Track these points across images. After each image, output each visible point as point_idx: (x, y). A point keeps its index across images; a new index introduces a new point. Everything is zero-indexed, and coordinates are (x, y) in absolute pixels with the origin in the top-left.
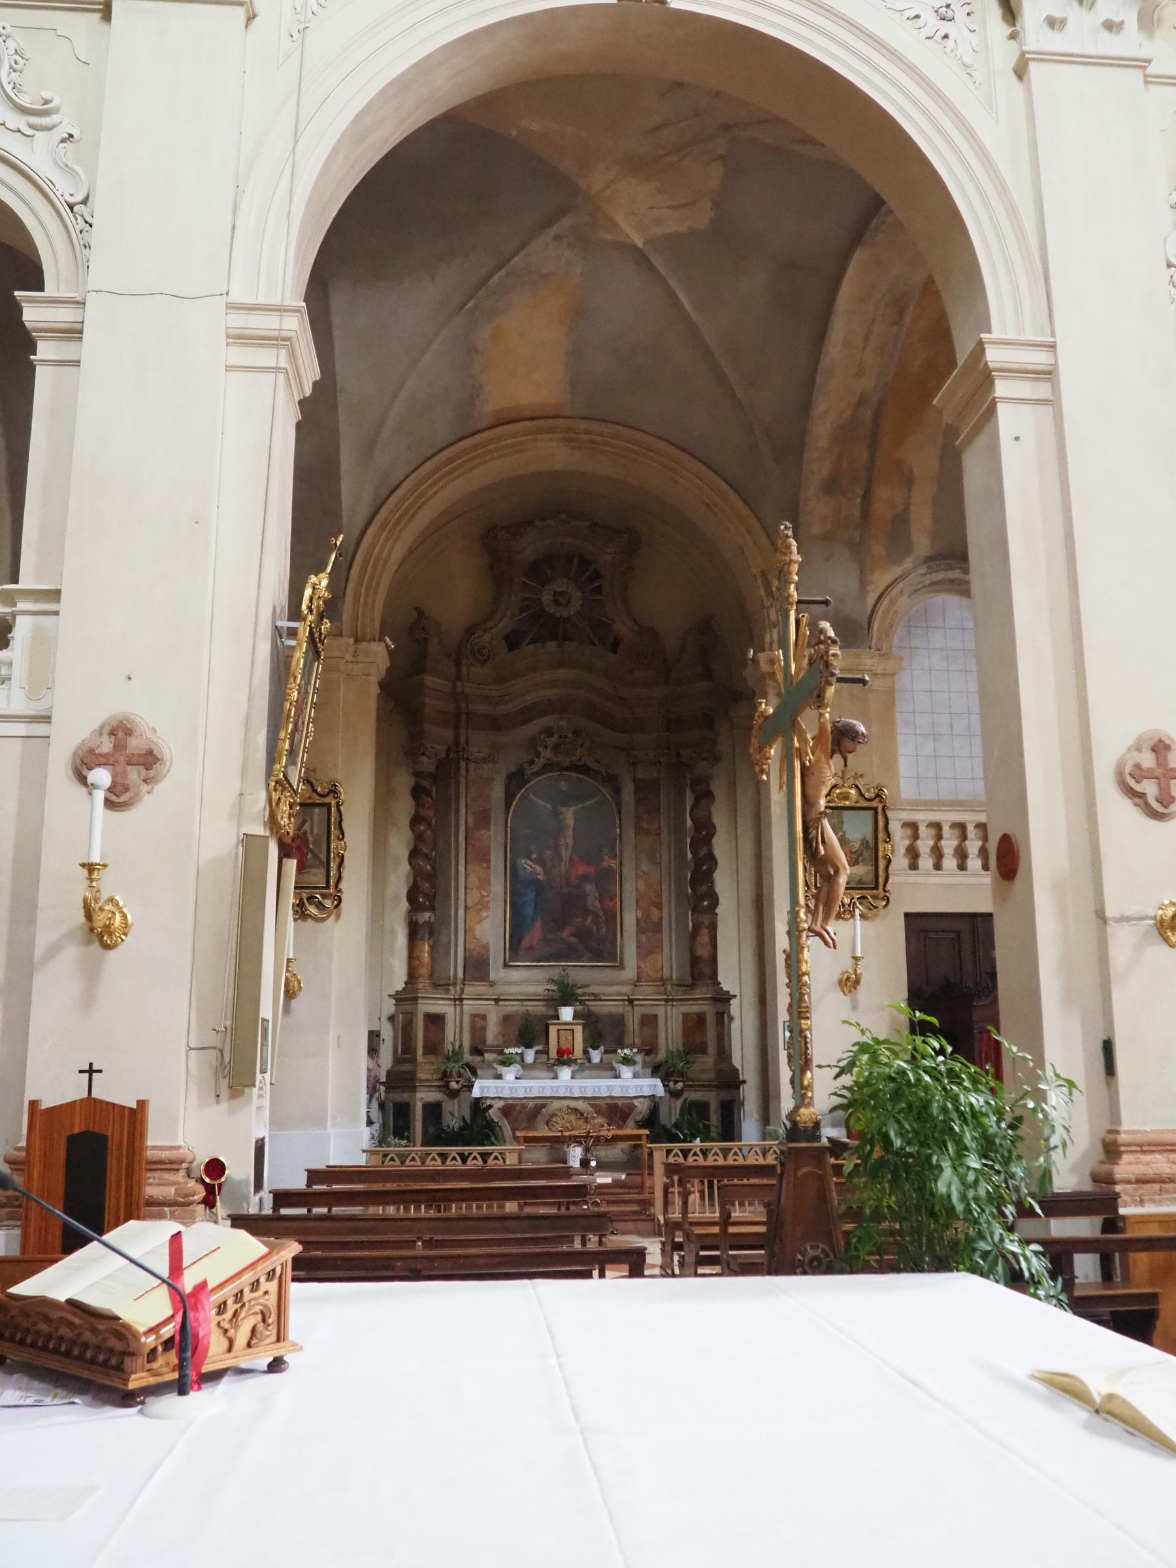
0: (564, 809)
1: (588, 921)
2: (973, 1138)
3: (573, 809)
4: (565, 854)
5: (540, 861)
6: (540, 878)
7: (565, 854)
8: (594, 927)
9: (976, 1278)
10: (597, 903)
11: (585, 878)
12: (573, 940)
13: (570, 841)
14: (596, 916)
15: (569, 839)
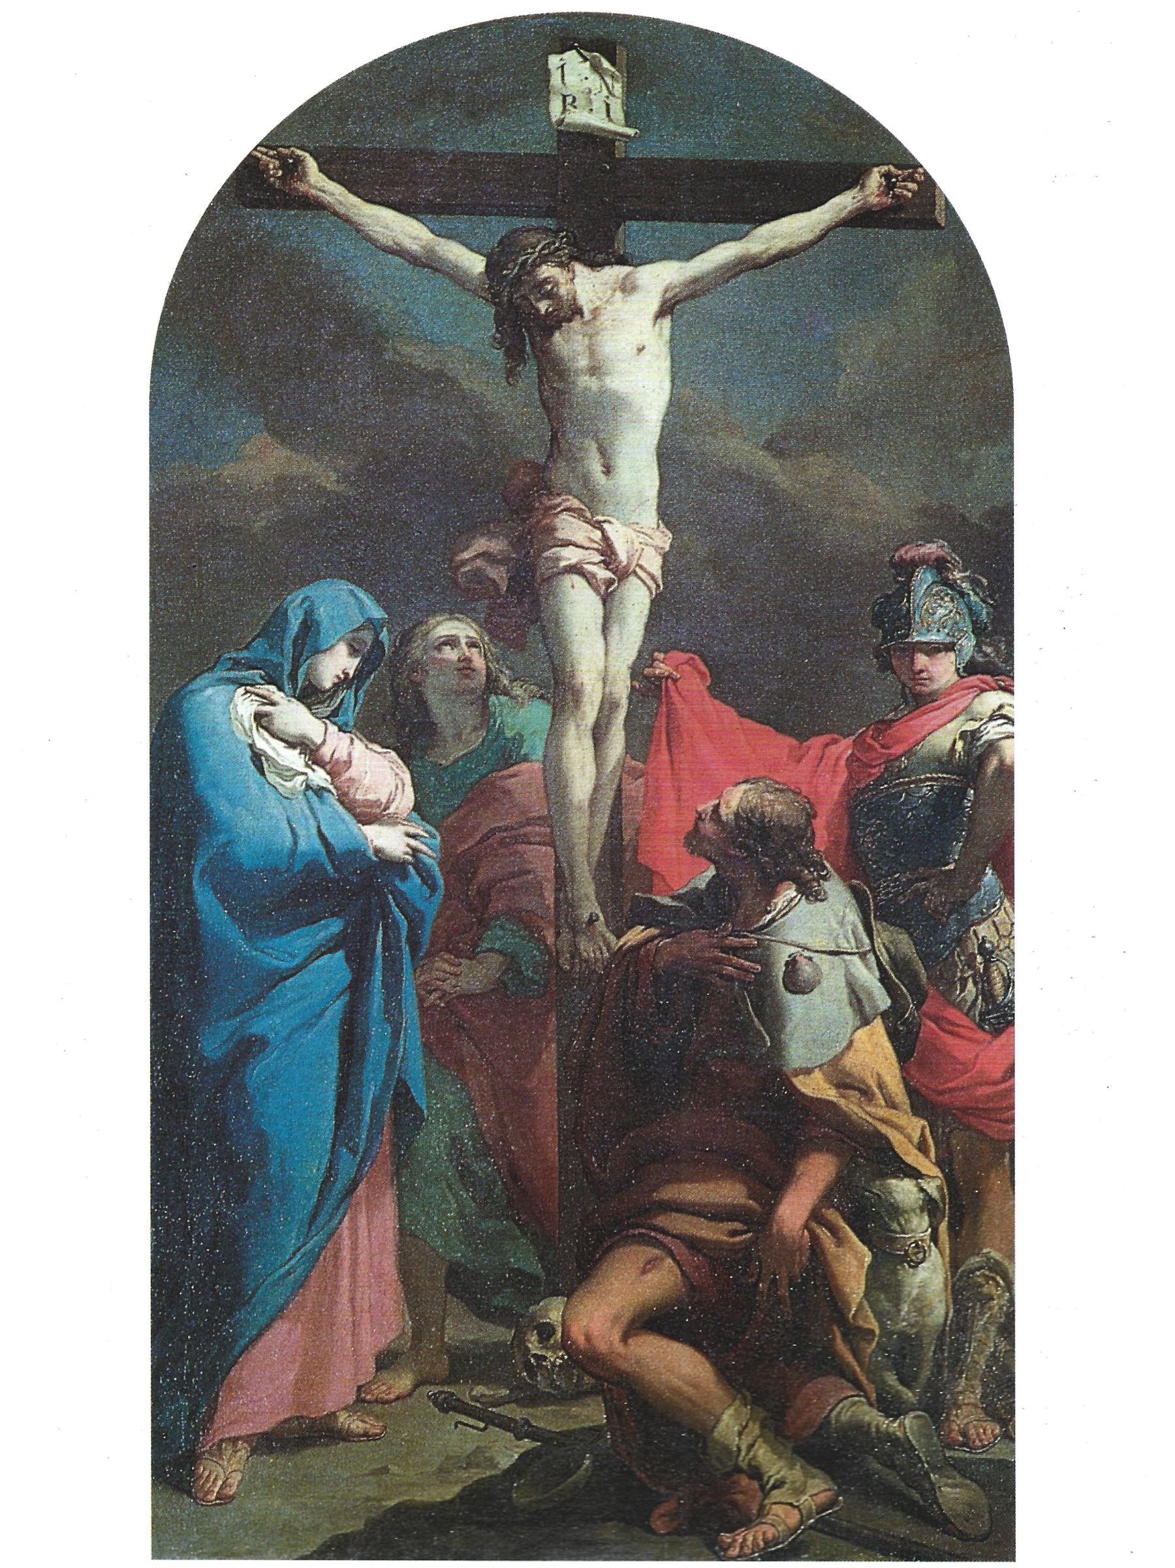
0: (587, 285)
1: (793, 1211)
2: (988, 613)
3: (660, 277)
4: (601, 644)
5: (393, 709)
6: (390, 840)
7: (601, 644)
8: (852, 1263)
9: (551, 11)
10: (873, 1051)
11: (764, 856)
12: (677, 1366)
13: (639, 532)
14: (873, 1156)
15: (627, 515)
